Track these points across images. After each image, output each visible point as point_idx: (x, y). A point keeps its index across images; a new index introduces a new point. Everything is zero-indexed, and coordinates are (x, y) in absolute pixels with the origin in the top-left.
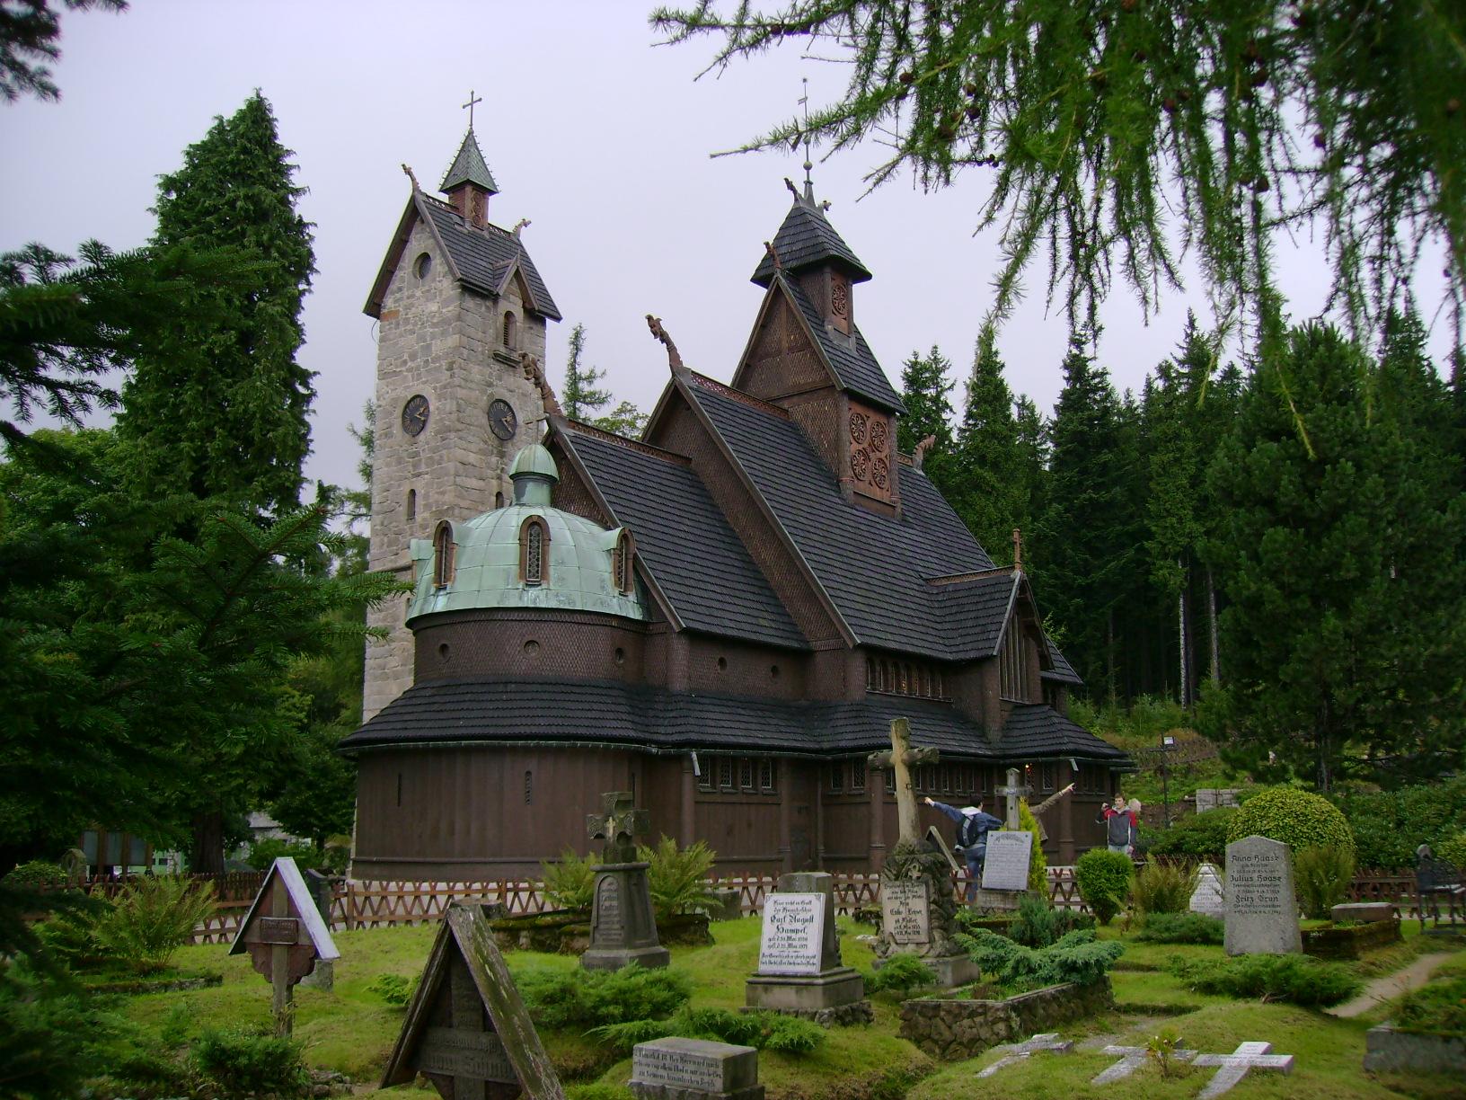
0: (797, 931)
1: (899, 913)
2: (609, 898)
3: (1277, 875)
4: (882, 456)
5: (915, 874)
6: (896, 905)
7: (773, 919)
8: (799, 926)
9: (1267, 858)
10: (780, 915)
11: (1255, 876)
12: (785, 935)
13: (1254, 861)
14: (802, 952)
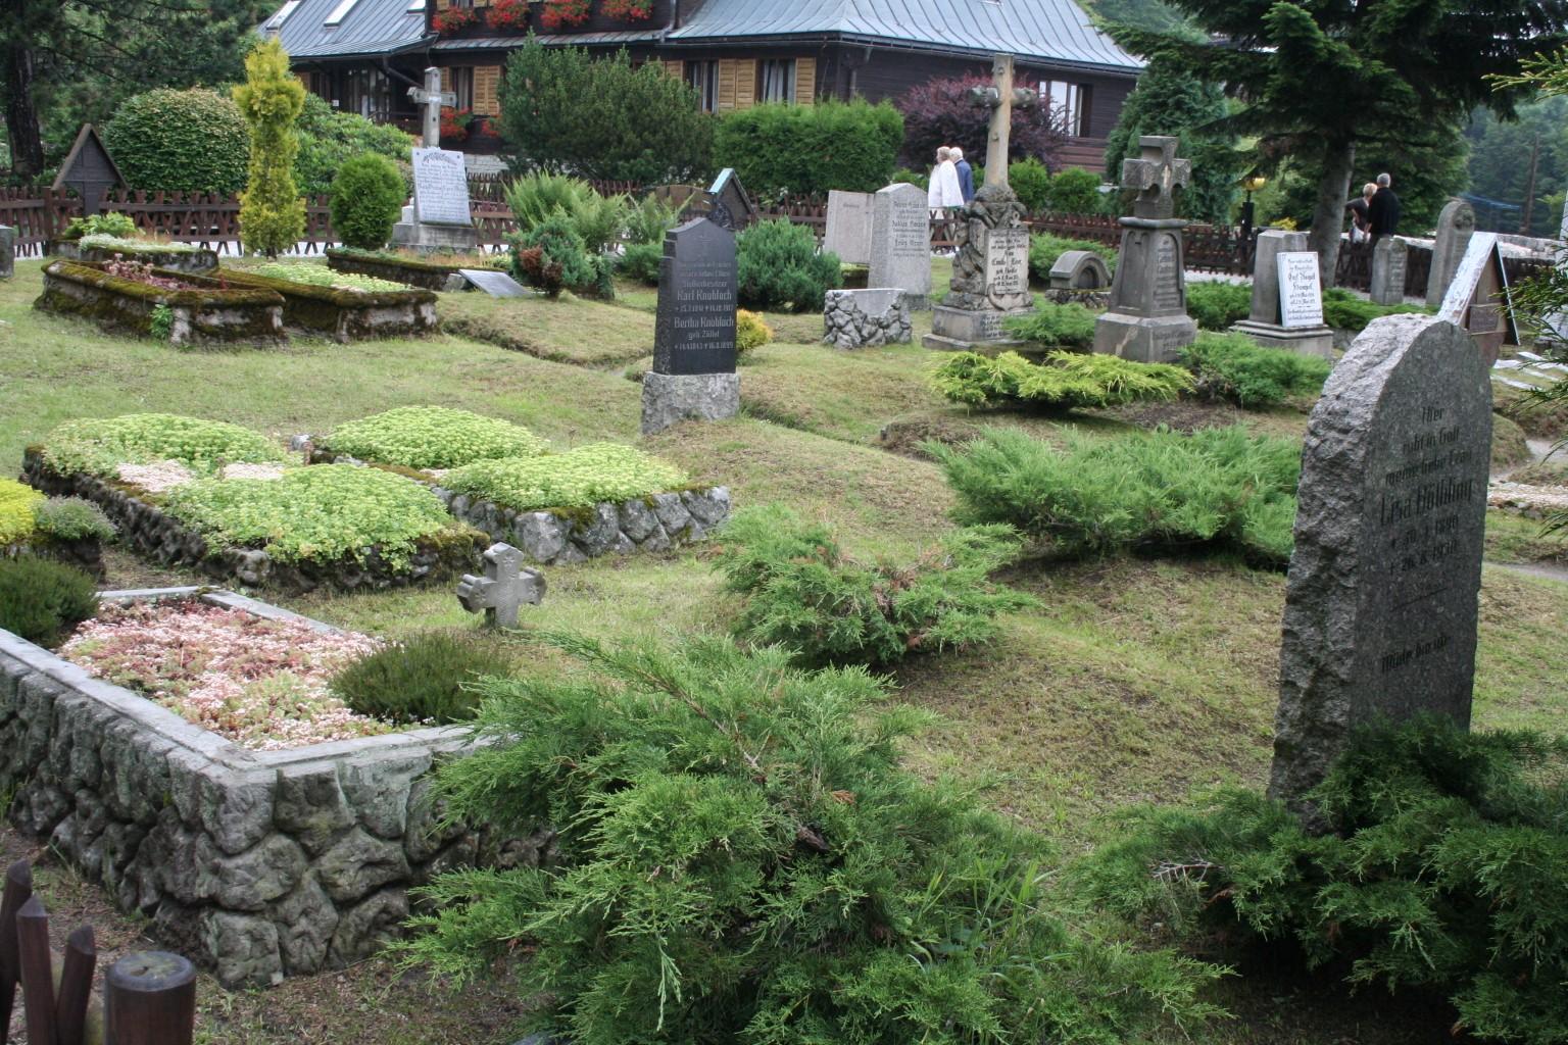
1: (1001, 263)
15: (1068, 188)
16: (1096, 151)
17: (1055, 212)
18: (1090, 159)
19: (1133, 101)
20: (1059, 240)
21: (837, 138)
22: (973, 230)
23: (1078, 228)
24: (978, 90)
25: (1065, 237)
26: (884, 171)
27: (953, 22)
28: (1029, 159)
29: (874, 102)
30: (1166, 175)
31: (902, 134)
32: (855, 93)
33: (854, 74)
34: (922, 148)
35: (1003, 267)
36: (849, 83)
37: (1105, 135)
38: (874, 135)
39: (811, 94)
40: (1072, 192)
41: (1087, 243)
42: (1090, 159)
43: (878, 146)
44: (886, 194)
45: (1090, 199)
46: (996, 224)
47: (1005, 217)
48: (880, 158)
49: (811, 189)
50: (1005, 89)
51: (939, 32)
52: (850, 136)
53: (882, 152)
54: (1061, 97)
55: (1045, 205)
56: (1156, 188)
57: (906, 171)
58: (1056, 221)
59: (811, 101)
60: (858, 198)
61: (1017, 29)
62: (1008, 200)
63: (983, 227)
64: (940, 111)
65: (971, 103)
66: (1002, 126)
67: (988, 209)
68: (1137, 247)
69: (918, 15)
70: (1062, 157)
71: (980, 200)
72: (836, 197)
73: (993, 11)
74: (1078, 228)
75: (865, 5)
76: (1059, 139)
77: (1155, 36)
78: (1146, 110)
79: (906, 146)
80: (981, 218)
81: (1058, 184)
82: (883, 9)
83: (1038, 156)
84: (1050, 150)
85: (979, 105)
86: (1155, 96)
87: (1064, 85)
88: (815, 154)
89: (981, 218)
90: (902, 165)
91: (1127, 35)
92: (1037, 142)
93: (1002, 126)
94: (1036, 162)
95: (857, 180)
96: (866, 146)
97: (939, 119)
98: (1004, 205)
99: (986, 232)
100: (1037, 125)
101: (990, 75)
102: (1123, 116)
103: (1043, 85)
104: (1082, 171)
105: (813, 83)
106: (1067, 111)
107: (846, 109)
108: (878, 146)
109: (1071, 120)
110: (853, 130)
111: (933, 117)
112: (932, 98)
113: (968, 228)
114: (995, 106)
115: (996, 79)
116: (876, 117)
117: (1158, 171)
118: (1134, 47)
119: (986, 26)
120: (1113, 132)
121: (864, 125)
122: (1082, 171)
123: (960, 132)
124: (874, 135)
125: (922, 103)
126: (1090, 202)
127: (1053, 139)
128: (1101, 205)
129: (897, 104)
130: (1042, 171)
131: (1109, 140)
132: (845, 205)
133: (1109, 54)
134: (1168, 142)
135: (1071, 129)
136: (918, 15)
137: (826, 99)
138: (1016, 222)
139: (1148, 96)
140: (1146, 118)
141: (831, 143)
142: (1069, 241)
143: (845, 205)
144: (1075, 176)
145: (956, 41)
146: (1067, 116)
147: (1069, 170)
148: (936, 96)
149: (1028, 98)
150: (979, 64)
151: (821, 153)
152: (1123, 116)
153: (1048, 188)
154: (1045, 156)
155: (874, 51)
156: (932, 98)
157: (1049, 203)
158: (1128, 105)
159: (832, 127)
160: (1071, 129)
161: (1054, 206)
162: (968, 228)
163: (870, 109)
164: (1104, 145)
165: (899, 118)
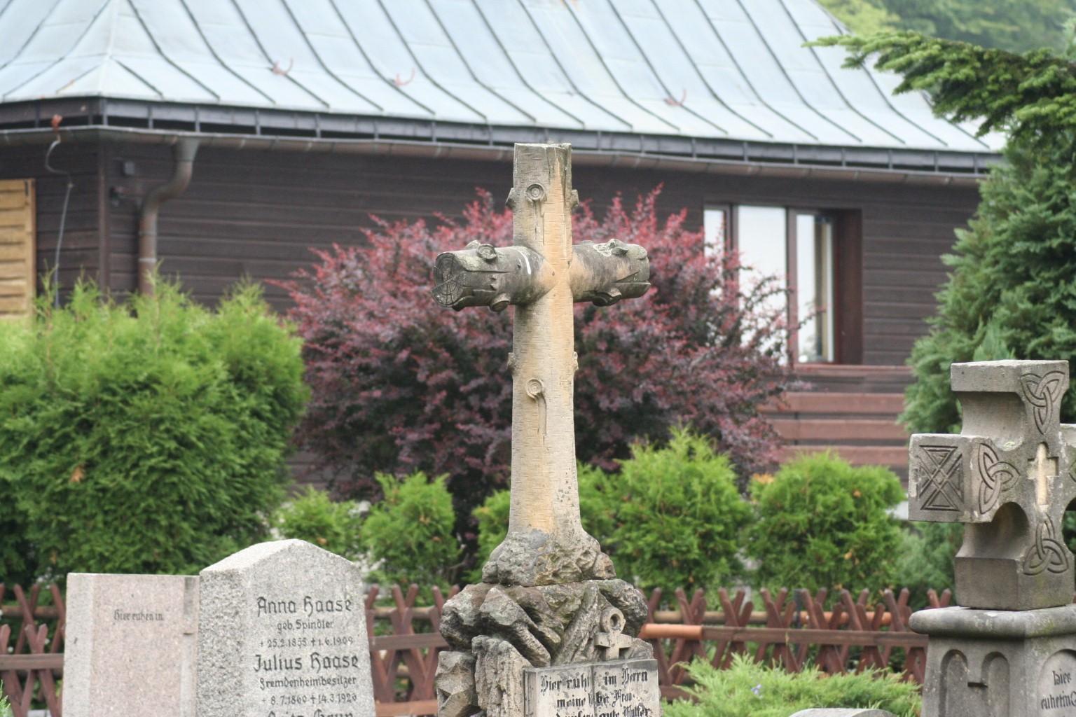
3: (348, 650)
9: (328, 606)
11: (305, 654)
15: (802, 517)
16: (882, 401)
17: (773, 589)
18: (869, 428)
19: (978, 253)
20: (779, 677)
21: (97, 414)
22: (485, 670)
23: (838, 636)
24: (469, 256)
25: (793, 667)
26: (251, 499)
27: (436, 53)
28: (681, 439)
29: (211, 302)
30: (1042, 473)
31: (299, 389)
32: (151, 278)
33: (151, 221)
34: (361, 427)
36: (135, 248)
37: (901, 352)
38: (214, 396)
39: (26, 285)
40: (814, 528)
41: (864, 680)
42: (869, 428)
43: (227, 428)
44: (230, 576)
45: (866, 549)
46: (554, 650)
47: (582, 628)
48: (237, 462)
49: (33, 566)
50: (550, 246)
51: (393, 84)
52: (141, 403)
53: (242, 444)
54: (770, 259)
55: (736, 568)
56: (1013, 518)
57: (317, 499)
58: (772, 619)
59: (27, 303)
60: (159, 590)
61: (625, 64)
62: (586, 574)
63: (517, 661)
64: (406, 314)
65: (452, 294)
66: (549, 359)
67: (529, 609)
68: (973, 697)
69: (332, 43)
70: (783, 426)
71: (504, 580)
72: (89, 597)
73: (553, 19)
74: (838, 636)
75: (170, 20)
76: (763, 376)
77: (1015, 62)
78: (1016, 277)
79: (314, 421)
80: (508, 633)
81: (774, 507)
82: (225, 28)
83: (707, 428)
84: (738, 409)
85: (476, 297)
86: (1037, 232)
87: (776, 216)
88: (38, 465)
89: (508, 633)
90: (302, 479)
91: (933, 64)
92: (699, 388)
93: (549, 359)
94: (702, 447)
95: (171, 531)
96: (191, 431)
97: (406, 338)
98: (576, 590)
99: (526, 676)
100: (700, 338)
101: (503, 205)
102: (949, 295)
103: (713, 220)
104: (836, 462)
105: (28, 252)
106: (791, 292)
107: (125, 324)
108: (227, 428)
109: (805, 306)
110: (148, 386)
111: (386, 333)
112: (372, 285)
113: (470, 666)
114: (525, 299)
115: (522, 220)
116: (217, 343)
117: (1017, 465)
118: (955, 97)
119: (533, 61)
120: (923, 344)
121: (180, 368)
122: (836, 462)
123: (471, 374)
124: (214, 396)
125: (354, 294)
126: (869, 558)
127: (748, 375)
128: (905, 562)
129: (279, 303)
130: (720, 471)
131: (914, 367)
132: (119, 615)
133: (908, 124)
134: (1036, 376)
135: (806, 338)
136: (332, 43)
137: (64, 299)
138: (617, 640)
139: (1017, 234)
140: (1017, 298)
141: (86, 427)
142: (810, 677)
143: (119, 615)
144: (821, 482)
145: (447, 110)
146: (791, 306)
147: (801, 466)
148: (392, 272)
149: (622, 270)
150: (463, 173)
151: (56, 460)
152: (949, 295)
153: (743, 521)
154: (727, 426)
155: (205, 151)
156: (372, 285)
157: (750, 564)
158: (966, 260)
159: (87, 384)
160: (806, 338)
161: (765, 574)
162: (470, 666)
163: (199, 321)
164: (901, 384)
165: (286, 344)
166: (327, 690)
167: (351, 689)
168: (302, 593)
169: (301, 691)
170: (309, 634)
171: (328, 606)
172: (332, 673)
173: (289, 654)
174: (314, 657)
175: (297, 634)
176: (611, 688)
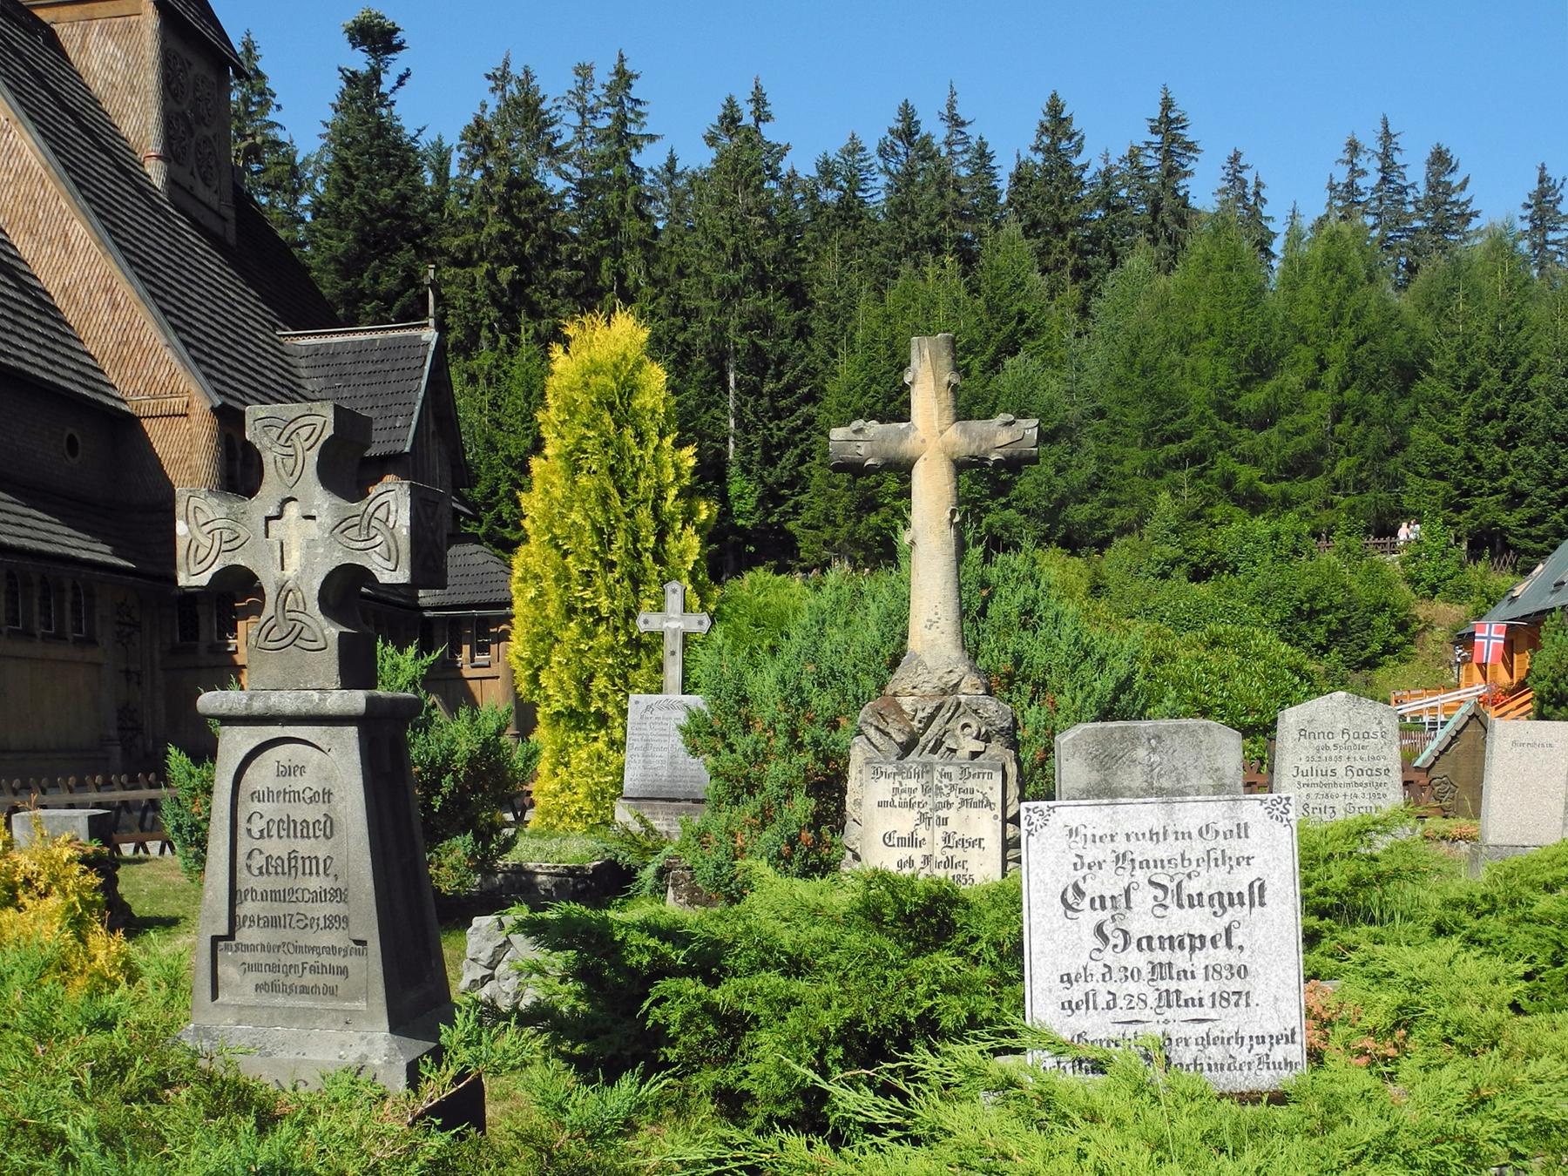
0: (1197, 942)
1: (912, 841)
2: (290, 827)
3: (1381, 764)
4: (210, 133)
5: (970, 745)
6: (904, 822)
7: (1073, 896)
8: (1200, 921)
9: (1366, 735)
10: (1106, 883)
11: (1341, 771)
12: (1136, 959)
13: (1339, 739)
14: (1229, 1021)
35: (917, 854)
166: (1359, 791)
167: (1382, 790)
168: (1341, 726)
169: (1334, 791)
170: (1345, 753)
171: (1366, 735)
172: (1365, 779)
173: (1323, 766)
174: (1349, 768)
175: (1334, 753)
176: (946, 781)
